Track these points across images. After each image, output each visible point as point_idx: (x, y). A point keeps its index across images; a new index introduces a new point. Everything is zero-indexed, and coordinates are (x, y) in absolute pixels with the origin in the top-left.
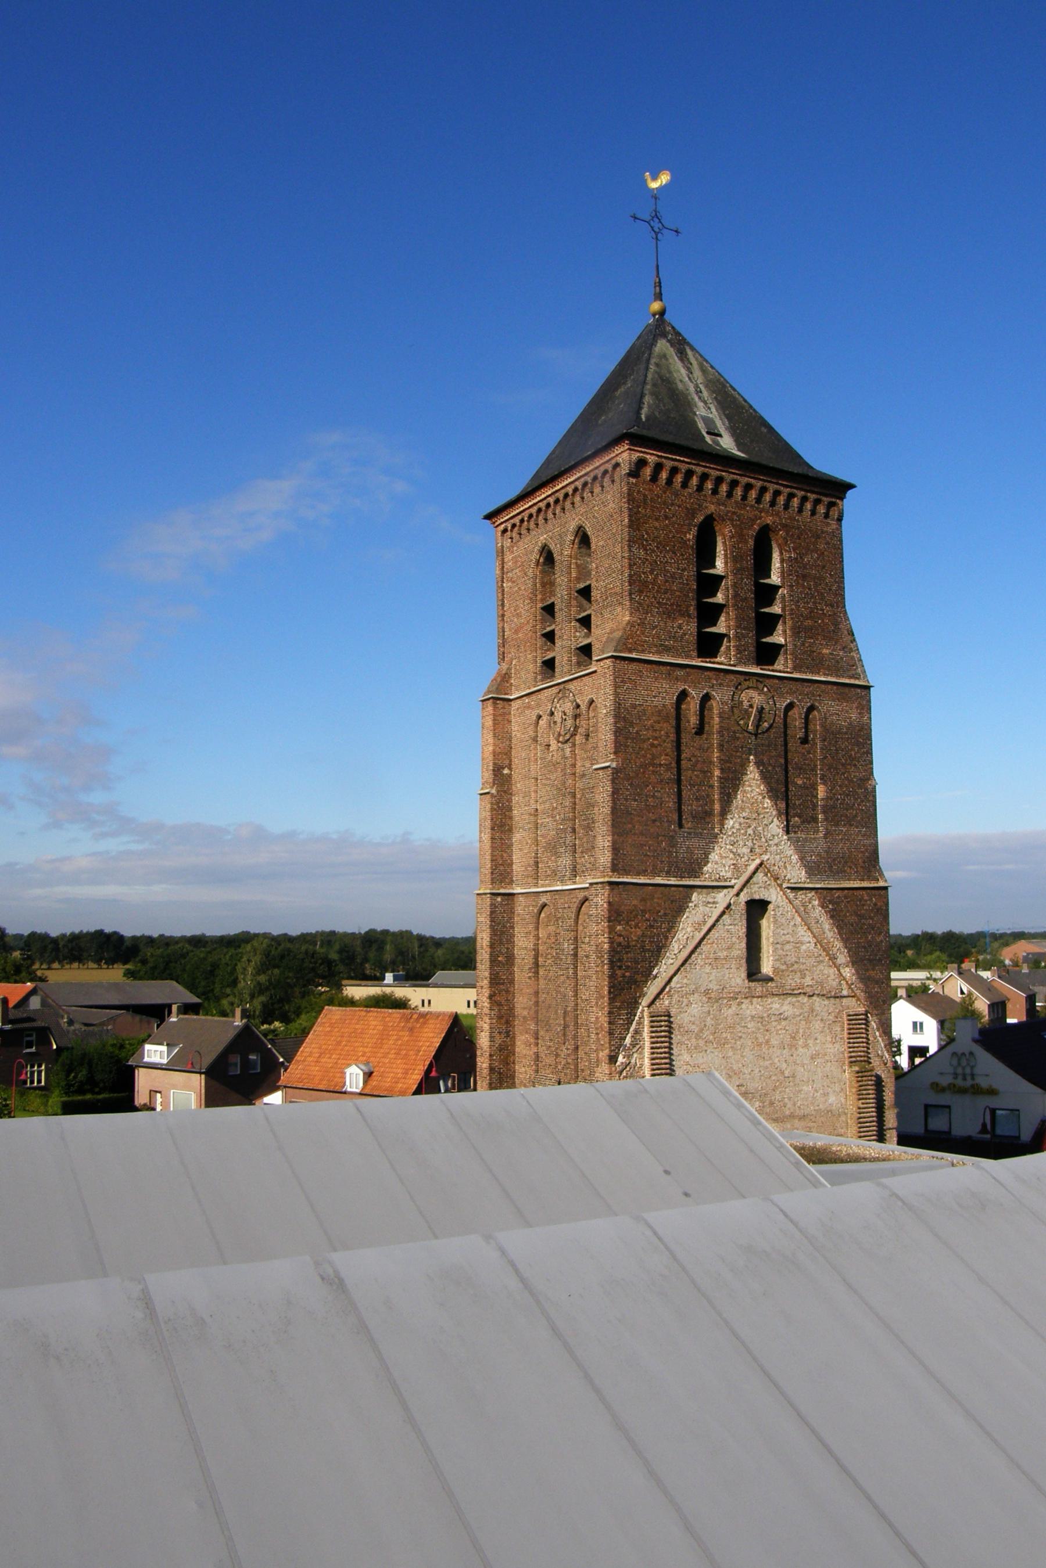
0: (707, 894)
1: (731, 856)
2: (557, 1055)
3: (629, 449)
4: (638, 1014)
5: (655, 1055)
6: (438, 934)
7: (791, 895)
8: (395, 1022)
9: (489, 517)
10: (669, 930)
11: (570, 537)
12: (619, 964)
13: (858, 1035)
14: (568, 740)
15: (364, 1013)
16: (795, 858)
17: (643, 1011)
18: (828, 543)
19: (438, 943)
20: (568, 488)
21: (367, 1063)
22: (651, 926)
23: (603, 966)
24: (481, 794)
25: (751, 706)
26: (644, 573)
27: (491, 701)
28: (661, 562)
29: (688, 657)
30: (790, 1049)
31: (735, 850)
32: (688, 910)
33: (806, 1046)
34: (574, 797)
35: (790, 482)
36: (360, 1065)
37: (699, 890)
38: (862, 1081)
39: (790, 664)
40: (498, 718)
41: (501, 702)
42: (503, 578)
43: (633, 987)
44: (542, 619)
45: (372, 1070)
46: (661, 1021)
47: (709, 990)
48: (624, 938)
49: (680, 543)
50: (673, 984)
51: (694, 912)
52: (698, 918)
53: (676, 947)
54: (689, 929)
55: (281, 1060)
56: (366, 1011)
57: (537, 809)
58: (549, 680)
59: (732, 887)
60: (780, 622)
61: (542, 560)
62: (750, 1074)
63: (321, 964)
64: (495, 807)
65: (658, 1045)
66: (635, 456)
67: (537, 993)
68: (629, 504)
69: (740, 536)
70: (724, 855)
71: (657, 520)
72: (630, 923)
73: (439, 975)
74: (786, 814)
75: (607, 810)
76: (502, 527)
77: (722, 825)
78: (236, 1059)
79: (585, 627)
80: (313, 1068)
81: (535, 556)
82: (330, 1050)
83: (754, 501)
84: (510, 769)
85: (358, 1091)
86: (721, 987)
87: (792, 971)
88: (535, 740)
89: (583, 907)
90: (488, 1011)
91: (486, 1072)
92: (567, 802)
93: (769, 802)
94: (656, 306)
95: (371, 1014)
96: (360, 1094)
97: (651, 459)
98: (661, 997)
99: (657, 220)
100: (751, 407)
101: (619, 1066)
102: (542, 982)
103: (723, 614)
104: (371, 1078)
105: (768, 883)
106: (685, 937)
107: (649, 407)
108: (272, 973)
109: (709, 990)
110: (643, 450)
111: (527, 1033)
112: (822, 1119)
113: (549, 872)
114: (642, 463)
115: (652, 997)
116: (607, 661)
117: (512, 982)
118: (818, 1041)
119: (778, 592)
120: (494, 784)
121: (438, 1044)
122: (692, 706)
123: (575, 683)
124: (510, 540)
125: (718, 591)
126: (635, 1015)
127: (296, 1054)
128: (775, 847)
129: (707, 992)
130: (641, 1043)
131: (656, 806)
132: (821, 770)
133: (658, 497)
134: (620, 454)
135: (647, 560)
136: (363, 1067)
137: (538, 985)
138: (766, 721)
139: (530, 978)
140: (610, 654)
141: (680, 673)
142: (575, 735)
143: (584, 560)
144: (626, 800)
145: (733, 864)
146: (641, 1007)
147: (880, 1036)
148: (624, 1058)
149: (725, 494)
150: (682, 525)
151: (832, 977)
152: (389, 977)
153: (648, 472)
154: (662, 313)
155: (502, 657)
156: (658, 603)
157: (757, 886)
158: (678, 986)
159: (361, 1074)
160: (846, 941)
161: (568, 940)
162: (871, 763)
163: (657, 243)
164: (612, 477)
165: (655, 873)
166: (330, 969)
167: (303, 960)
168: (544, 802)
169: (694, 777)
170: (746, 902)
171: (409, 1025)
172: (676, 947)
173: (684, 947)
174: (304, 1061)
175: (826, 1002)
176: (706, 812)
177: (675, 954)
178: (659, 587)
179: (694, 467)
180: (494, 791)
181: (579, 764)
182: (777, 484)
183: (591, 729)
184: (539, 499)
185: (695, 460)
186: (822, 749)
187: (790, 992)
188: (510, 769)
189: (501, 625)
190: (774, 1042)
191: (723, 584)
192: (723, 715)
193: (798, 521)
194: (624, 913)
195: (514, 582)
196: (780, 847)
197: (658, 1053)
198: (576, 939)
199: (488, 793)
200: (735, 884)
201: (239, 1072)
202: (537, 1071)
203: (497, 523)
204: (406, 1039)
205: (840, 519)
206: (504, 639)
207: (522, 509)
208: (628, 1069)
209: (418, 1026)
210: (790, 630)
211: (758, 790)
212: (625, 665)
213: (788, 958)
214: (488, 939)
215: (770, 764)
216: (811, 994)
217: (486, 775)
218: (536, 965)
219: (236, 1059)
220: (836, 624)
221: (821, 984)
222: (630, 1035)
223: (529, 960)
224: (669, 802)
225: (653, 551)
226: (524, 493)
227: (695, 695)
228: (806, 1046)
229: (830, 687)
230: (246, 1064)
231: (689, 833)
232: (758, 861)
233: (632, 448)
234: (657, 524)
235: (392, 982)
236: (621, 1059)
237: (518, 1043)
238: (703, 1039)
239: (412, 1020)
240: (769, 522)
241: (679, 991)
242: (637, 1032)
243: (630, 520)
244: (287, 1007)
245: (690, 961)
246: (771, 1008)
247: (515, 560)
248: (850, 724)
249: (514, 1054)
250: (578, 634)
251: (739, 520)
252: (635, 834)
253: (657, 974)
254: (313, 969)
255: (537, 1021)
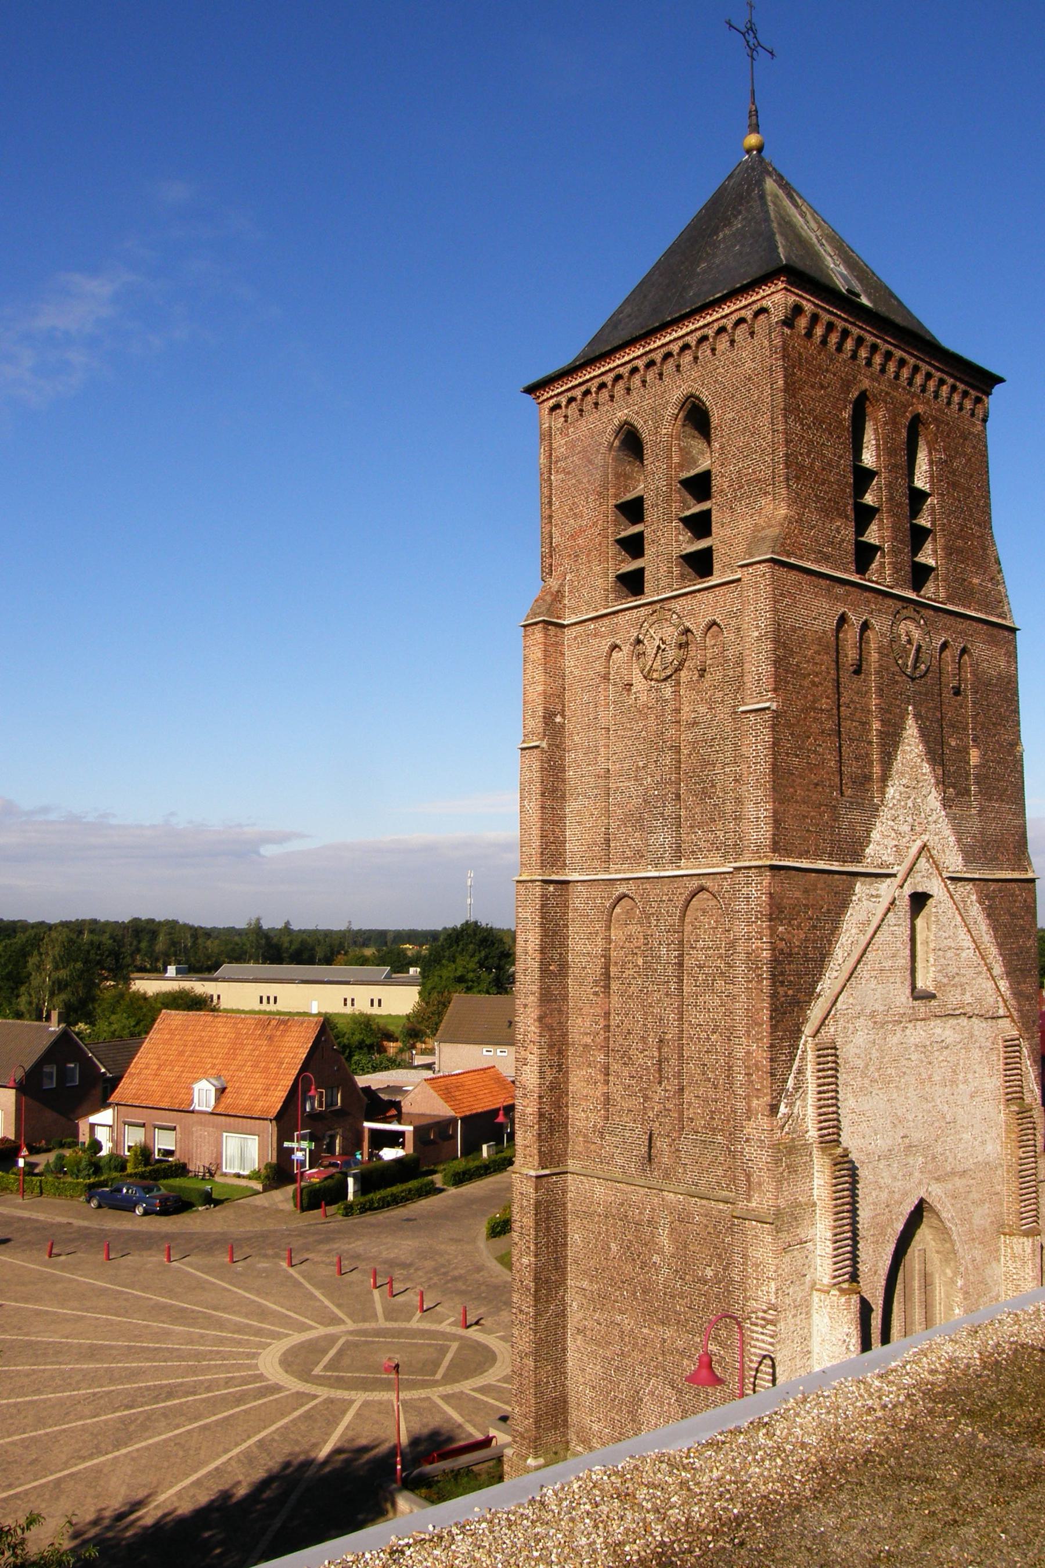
0: (871, 884)
1: (893, 835)
2: (646, 1098)
3: (785, 289)
4: (801, 1046)
5: (822, 1102)
6: (208, 924)
7: (951, 887)
8: (249, 1029)
9: (530, 390)
10: (832, 933)
11: (672, 410)
12: (781, 978)
13: (1014, 1065)
14: (671, 676)
15: (210, 1019)
16: (952, 839)
17: (806, 1041)
18: (974, 447)
19: (208, 933)
20: (671, 346)
21: (218, 1077)
22: (814, 927)
23: (760, 982)
24: (523, 749)
25: (909, 642)
26: (801, 454)
27: (541, 625)
28: (818, 443)
29: (846, 571)
30: (951, 1086)
31: (896, 828)
32: (851, 905)
33: (966, 1081)
34: (678, 751)
35: (942, 364)
36: (211, 1080)
37: (863, 879)
38: (1022, 1124)
39: (942, 594)
40: (550, 649)
41: (553, 628)
42: (550, 469)
43: (796, 1010)
44: (615, 521)
45: (225, 1085)
46: (828, 1055)
47: (875, 1012)
48: (786, 944)
49: (836, 421)
50: (838, 1005)
51: (857, 908)
52: (863, 917)
53: (840, 955)
54: (854, 931)
55: (103, 1070)
56: (213, 1015)
57: (609, 770)
58: (624, 601)
59: (894, 875)
60: (930, 539)
61: (617, 443)
62: (914, 1121)
63: (107, 956)
64: (546, 765)
65: (825, 1088)
66: (792, 299)
67: (607, 1014)
68: (784, 360)
69: (893, 422)
70: (885, 833)
71: (812, 387)
72: (792, 922)
73: (226, 969)
74: (943, 782)
75: (764, 767)
76: (551, 402)
77: (883, 793)
78: (51, 1069)
79: (689, 529)
80: (151, 1083)
81: (608, 436)
82: (172, 1061)
83: (906, 382)
84: (563, 716)
85: (210, 1110)
86: (886, 1008)
87: (953, 985)
88: (606, 678)
89: (694, 899)
90: (537, 1038)
91: (532, 1119)
92: (668, 759)
93: (927, 766)
94: (753, 140)
95: (219, 1019)
96: (212, 1114)
97: (808, 307)
98: (827, 1022)
99: (752, 35)
100: (874, 274)
101: (781, 1119)
102: (615, 999)
103: (875, 522)
104: (225, 1095)
105: (930, 871)
106: (850, 942)
107: (784, 247)
108: (74, 968)
109: (875, 1012)
110: (800, 293)
111: (589, 1066)
112: (982, 1174)
113: (629, 854)
114: (798, 310)
115: (817, 1023)
116: (762, 567)
117: (565, 998)
118: (977, 1075)
119: (926, 501)
120: (545, 735)
121: (305, 1055)
122: (851, 635)
123: (682, 601)
124: (563, 419)
125: (866, 492)
126: (798, 1049)
127: (129, 1067)
128: (934, 826)
129: (872, 1015)
130: (805, 1085)
131: (818, 765)
132: (973, 729)
133: (813, 358)
134: (768, 295)
135: (804, 437)
136: (215, 1083)
137: (610, 1002)
138: (923, 662)
139: (596, 994)
140: (768, 556)
141: (840, 590)
142: (680, 670)
143: (687, 443)
144: (787, 754)
145: (896, 846)
146: (804, 1037)
147: (1031, 1066)
148: (786, 1107)
149: (878, 368)
150: (838, 399)
151: (990, 992)
152: (171, 970)
153: (803, 322)
154: (760, 149)
155: (548, 571)
156: (816, 495)
157: (919, 874)
158: (844, 1007)
159: (213, 1089)
160: (1000, 946)
161: (669, 944)
162: (1018, 724)
163: (752, 63)
164: (751, 327)
165: (818, 856)
166: (117, 961)
167: (88, 952)
168: (621, 761)
169: (853, 730)
170: (909, 896)
171: (268, 1033)
172: (840, 955)
173: (849, 954)
174: (139, 1074)
175: (984, 1025)
176: (865, 776)
177: (839, 965)
178: (816, 476)
179: (850, 326)
180: (544, 745)
181: (686, 709)
182: (929, 364)
183: (709, 662)
184: (618, 362)
185: (845, 314)
186: (974, 702)
187: (951, 1012)
188: (563, 716)
189: (546, 530)
190: (936, 1078)
191: (874, 482)
192: (881, 650)
193: (946, 414)
194: (786, 908)
195: (569, 473)
196: (939, 826)
197: (825, 1099)
198: (681, 942)
199: (537, 747)
200: (898, 871)
201: (54, 1086)
202: (607, 1118)
203: (541, 399)
204: (264, 1048)
205: (985, 420)
206: (551, 547)
207: (588, 377)
208: (790, 1122)
209: (278, 1033)
210: (943, 550)
211: (916, 750)
212: (782, 572)
213: (950, 968)
214: (537, 942)
215: (927, 719)
216: (971, 1014)
217: (531, 723)
218: (607, 975)
219: (51, 1069)
220: (984, 549)
221: (979, 1000)
222: (792, 1075)
223: (595, 969)
224: (830, 760)
225: (810, 428)
226: (572, 366)
227: (855, 619)
228: (966, 1081)
229: (980, 625)
230: (63, 1075)
231: (851, 803)
232: (919, 843)
233: (789, 287)
234: (813, 393)
235: (174, 975)
236: (783, 1109)
237: (573, 1079)
238: (868, 1077)
239: (270, 1027)
240: (920, 411)
241: (844, 1014)
242: (800, 1071)
243: (786, 382)
244: (91, 1007)
245: (856, 973)
246: (934, 1034)
247: (571, 445)
248: (999, 674)
249: (567, 1095)
250: (681, 538)
251: (892, 403)
252: (797, 802)
253: (821, 991)
254: (99, 962)
255: (606, 1049)
